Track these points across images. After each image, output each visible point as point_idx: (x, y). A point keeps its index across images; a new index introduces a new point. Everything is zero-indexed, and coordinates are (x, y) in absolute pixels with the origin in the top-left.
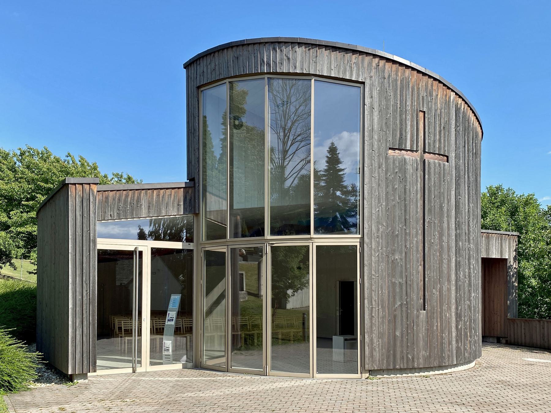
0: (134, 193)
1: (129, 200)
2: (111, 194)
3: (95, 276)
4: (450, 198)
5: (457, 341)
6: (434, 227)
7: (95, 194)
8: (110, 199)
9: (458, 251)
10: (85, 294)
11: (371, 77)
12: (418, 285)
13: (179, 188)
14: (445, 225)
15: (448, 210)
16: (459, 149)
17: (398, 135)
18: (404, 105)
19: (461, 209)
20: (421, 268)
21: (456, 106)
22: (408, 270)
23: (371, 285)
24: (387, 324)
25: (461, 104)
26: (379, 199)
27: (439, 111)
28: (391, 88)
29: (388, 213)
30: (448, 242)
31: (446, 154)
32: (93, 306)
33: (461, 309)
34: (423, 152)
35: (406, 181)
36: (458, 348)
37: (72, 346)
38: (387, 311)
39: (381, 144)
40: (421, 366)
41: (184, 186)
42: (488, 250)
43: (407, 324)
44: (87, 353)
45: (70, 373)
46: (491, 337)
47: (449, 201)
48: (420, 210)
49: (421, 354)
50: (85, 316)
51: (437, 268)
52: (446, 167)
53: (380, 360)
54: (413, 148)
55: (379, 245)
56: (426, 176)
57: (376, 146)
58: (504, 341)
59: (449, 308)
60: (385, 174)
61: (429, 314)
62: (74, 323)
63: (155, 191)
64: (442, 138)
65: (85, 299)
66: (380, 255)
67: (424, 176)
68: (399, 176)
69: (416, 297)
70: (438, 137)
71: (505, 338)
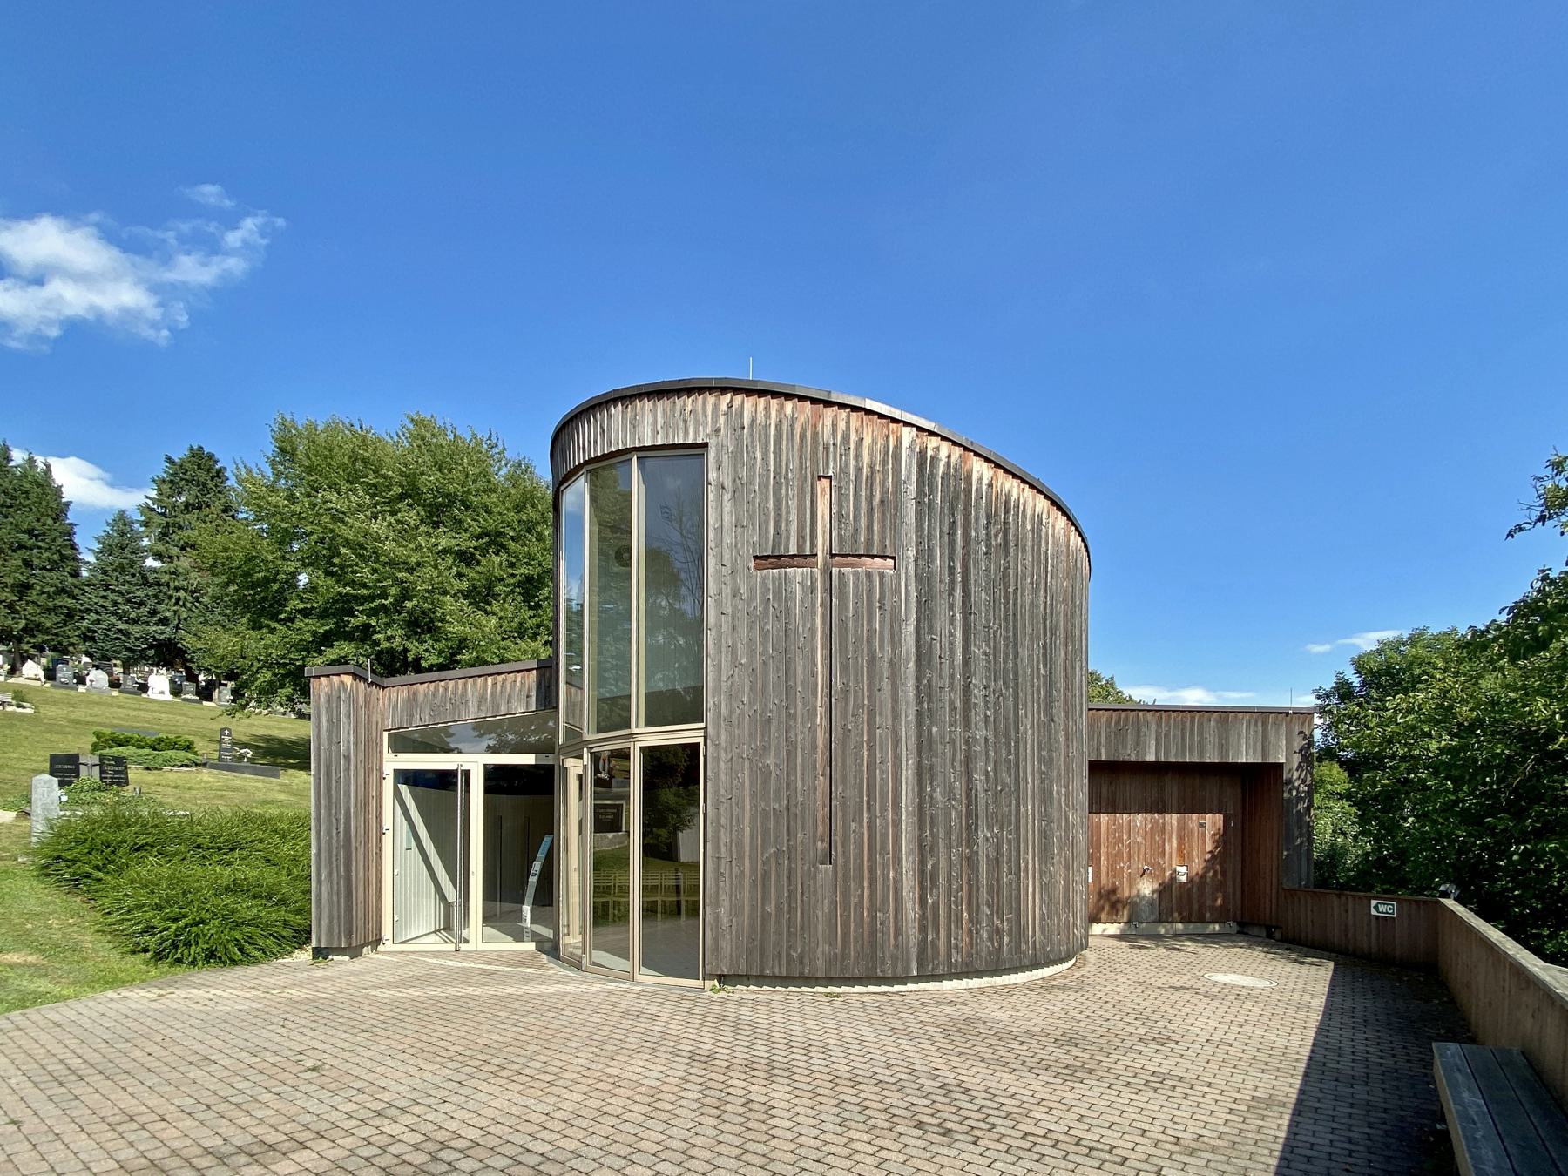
0: (456, 684)
5: (923, 929)
8: (421, 698)
13: (528, 670)
25: (938, 449)
27: (866, 471)
34: (828, 556)
36: (922, 944)
40: (819, 974)
42: (1223, 747)
46: (1256, 925)
49: (820, 949)
54: (804, 550)
64: (876, 523)
70: (863, 522)
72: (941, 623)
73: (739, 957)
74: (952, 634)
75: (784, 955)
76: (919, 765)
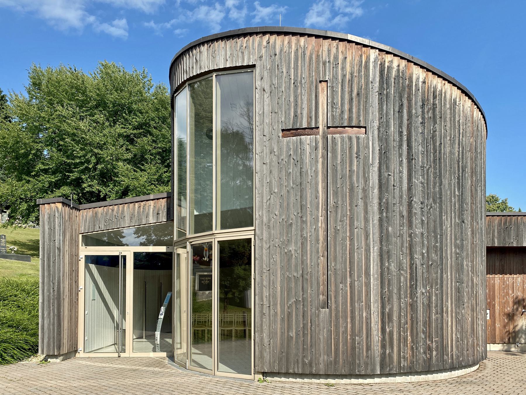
0: (118, 207)
17: (292, 114)
25: (391, 62)
29: (280, 201)
31: (362, 124)
34: (326, 128)
49: (321, 358)
52: (361, 141)
53: (272, 361)
54: (311, 125)
63: (137, 204)
64: (354, 107)
68: (293, 159)
70: (346, 107)
73: (274, 362)
75: (300, 361)
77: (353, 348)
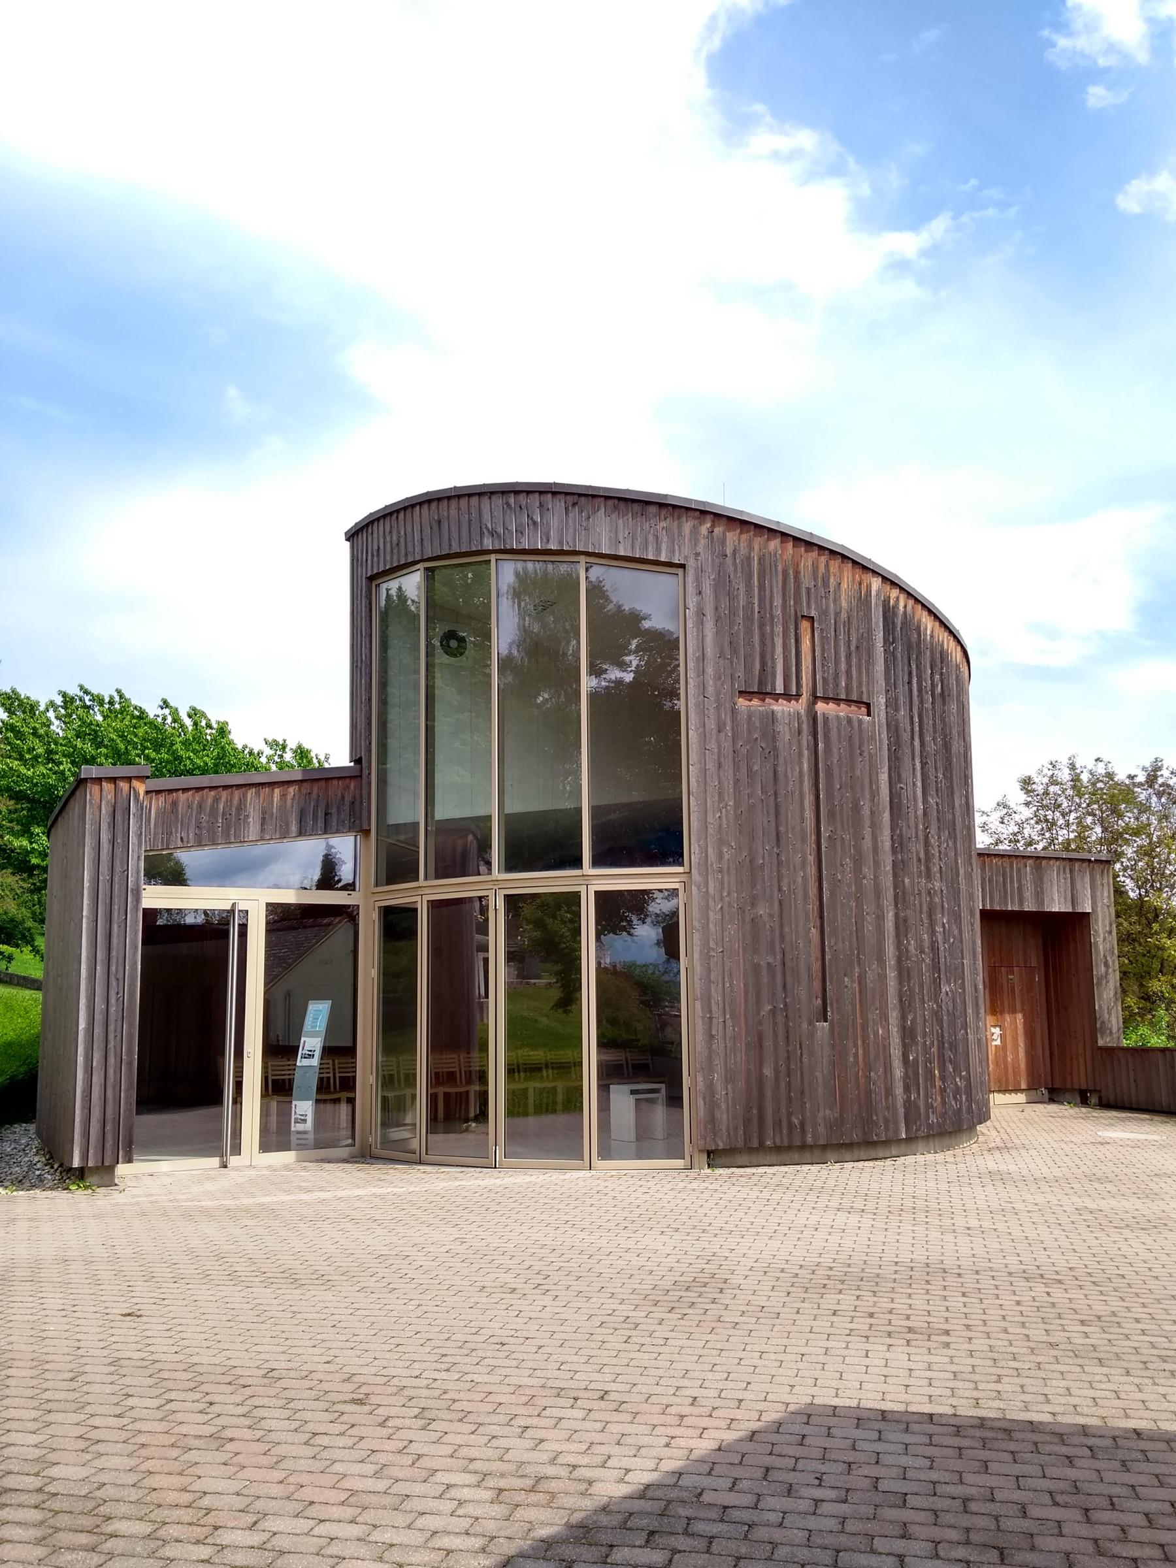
1: (221, 807)
2: (182, 797)
3: (136, 963)
4: (878, 788)
5: (907, 1089)
6: (843, 847)
7: (141, 798)
9: (900, 899)
10: (113, 1000)
11: (697, 554)
12: (809, 968)
14: (867, 843)
15: (872, 813)
16: (895, 688)
18: (768, 607)
19: (904, 809)
20: (814, 932)
21: (886, 602)
22: (787, 938)
23: (709, 970)
24: (744, 1051)
25: (898, 598)
26: (720, 794)
27: (844, 615)
28: (739, 574)
30: (876, 877)
32: (131, 1026)
33: (914, 1021)
35: (776, 757)
37: (83, 1108)
38: (743, 1025)
39: (722, 685)
41: (300, 778)
42: (1039, 895)
43: (788, 1051)
44: (113, 1123)
45: (76, 1163)
47: (874, 794)
48: (809, 814)
49: (821, 1114)
50: (111, 1044)
51: (851, 933)
52: (865, 726)
53: (731, 1126)
55: (723, 888)
56: (821, 746)
57: (710, 690)
58: (1094, 1100)
59: (885, 1017)
60: (731, 744)
61: (837, 1030)
62: (89, 1059)
64: (854, 669)
65: (112, 1009)
66: (726, 909)
67: (816, 745)
69: (805, 994)
70: (843, 666)
71: (1095, 1091)
72: (906, 773)
73: (736, 1128)
74: (914, 784)
75: (784, 1122)
76: (897, 916)
77: (869, 1093)
